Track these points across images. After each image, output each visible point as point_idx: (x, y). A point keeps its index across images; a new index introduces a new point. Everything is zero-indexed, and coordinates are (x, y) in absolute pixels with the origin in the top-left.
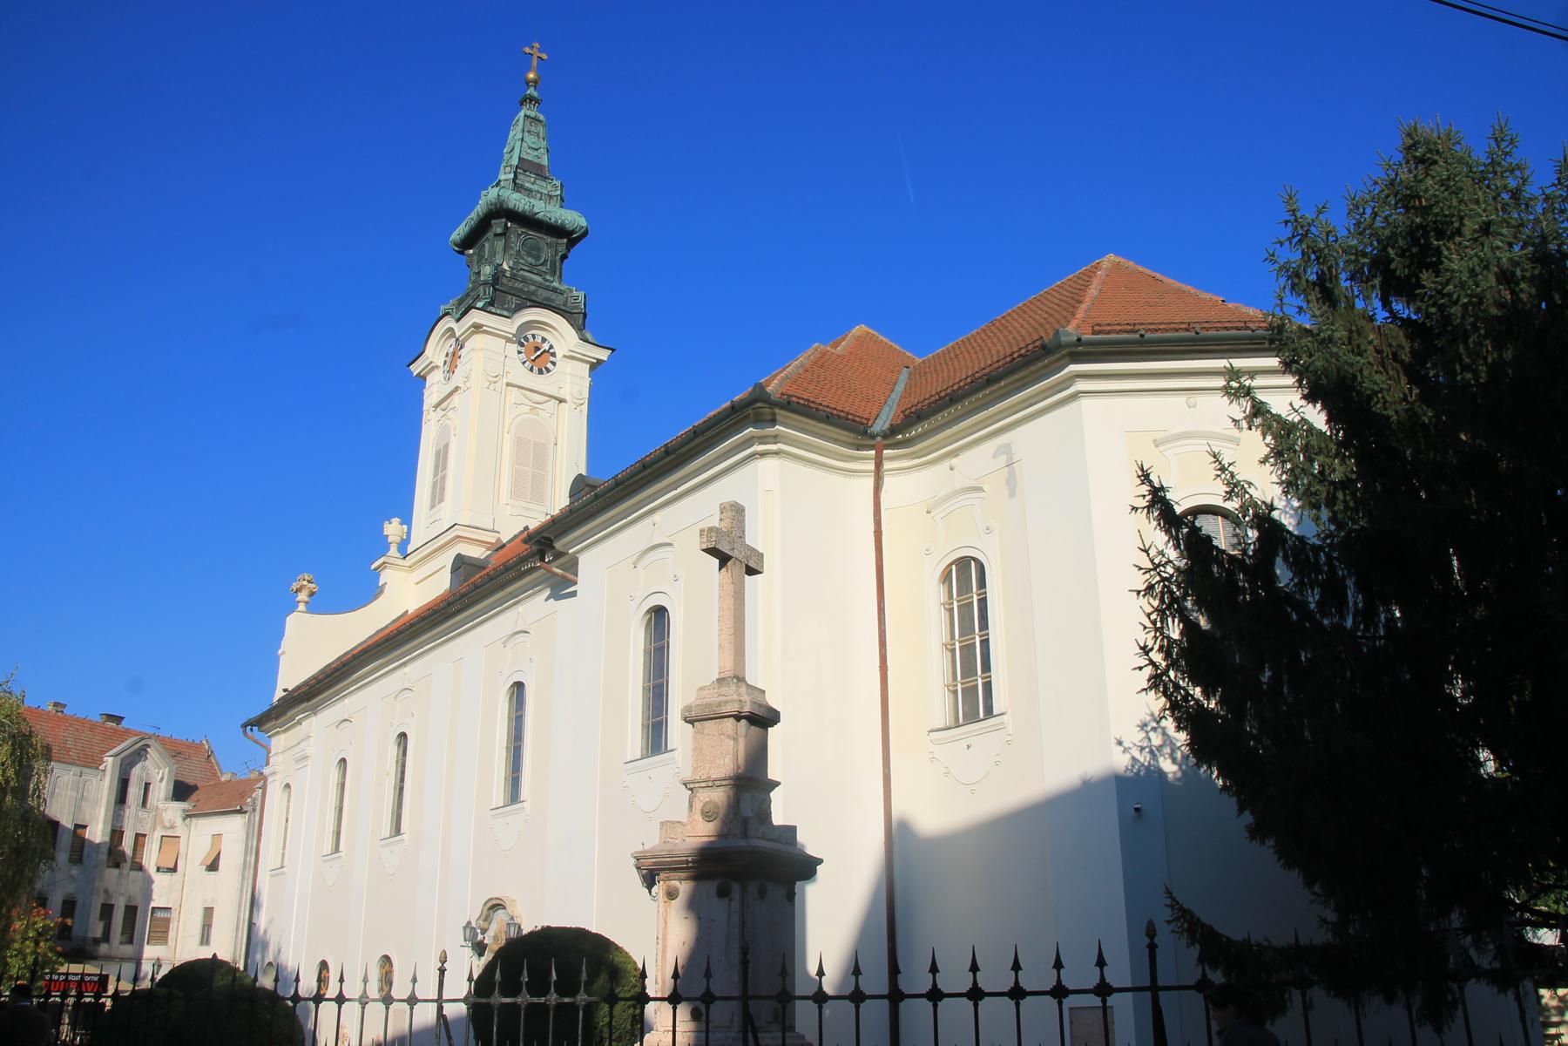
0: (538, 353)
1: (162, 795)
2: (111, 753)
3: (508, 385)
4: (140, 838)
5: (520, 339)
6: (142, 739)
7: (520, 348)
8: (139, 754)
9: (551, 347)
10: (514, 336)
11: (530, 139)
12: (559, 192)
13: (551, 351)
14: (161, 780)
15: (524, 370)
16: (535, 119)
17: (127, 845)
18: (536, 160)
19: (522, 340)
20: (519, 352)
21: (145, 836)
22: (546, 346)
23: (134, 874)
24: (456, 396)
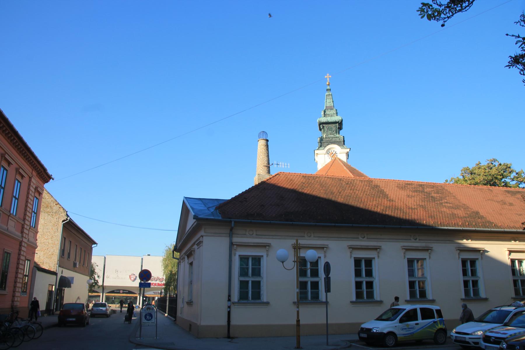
5: (328, 152)
9: (336, 152)
13: (336, 153)
18: (330, 105)
19: (329, 153)
20: (328, 156)
22: (334, 153)
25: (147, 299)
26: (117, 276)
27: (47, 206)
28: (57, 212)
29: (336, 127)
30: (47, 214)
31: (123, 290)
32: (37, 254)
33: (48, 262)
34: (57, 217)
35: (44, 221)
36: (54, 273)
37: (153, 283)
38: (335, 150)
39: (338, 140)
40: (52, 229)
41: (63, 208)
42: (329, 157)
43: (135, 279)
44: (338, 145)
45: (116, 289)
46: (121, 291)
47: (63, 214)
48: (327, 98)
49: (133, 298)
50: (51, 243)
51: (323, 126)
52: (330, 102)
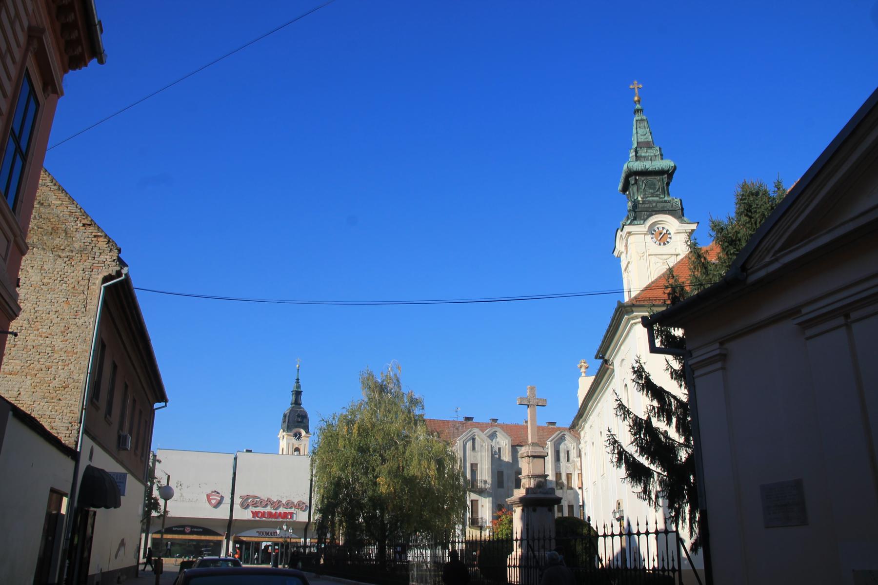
0: (661, 236)
1: (575, 455)
2: (549, 440)
3: (649, 255)
4: (569, 475)
5: (651, 231)
6: (561, 432)
7: (652, 236)
8: (562, 439)
9: (667, 230)
10: (647, 232)
11: (640, 131)
12: (659, 153)
13: (668, 232)
14: (574, 449)
15: (656, 246)
16: (642, 120)
17: (564, 479)
18: (646, 140)
20: (652, 238)
21: (571, 474)
22: (664, 231)
23: (569, 491)
24: (629, 265)
25: (244, 547)
26: (180, 495)
27: (52, 228)
28: (85, 249)
29: (661, 182)
30: (51, 255)
31: (192, 527)
32: (16, 335)
33: (48, 413)
34: (88, 264)
35: (40, 274)
36: (72, 454)
37: (257, 511)
38: (667, 227)
39: (668, 206)
40: (67, 302)
41: (106, 236)
42: (654, 239)
43: (220, 503)
44: (670, 214)
45: (175, 525)
46: (188, 530)
47: (108, 257)
48: (638, 127)
49: (212, 544)
50: (62, 349)
51: (636, 179)
52: (644, 134)
